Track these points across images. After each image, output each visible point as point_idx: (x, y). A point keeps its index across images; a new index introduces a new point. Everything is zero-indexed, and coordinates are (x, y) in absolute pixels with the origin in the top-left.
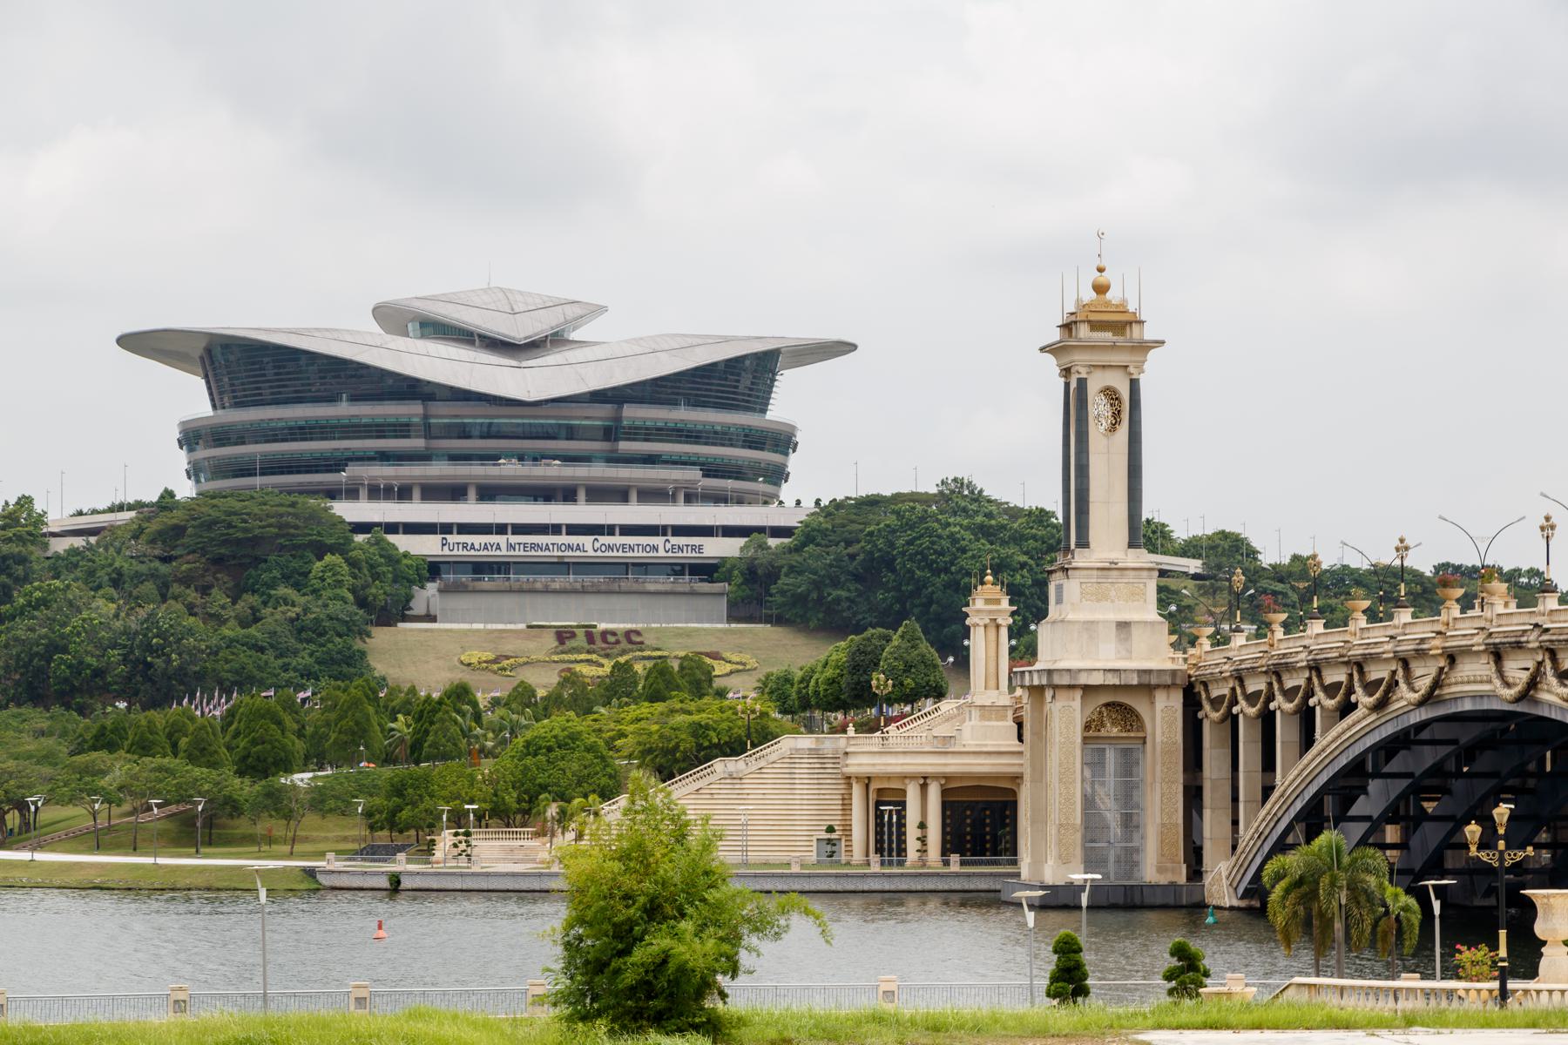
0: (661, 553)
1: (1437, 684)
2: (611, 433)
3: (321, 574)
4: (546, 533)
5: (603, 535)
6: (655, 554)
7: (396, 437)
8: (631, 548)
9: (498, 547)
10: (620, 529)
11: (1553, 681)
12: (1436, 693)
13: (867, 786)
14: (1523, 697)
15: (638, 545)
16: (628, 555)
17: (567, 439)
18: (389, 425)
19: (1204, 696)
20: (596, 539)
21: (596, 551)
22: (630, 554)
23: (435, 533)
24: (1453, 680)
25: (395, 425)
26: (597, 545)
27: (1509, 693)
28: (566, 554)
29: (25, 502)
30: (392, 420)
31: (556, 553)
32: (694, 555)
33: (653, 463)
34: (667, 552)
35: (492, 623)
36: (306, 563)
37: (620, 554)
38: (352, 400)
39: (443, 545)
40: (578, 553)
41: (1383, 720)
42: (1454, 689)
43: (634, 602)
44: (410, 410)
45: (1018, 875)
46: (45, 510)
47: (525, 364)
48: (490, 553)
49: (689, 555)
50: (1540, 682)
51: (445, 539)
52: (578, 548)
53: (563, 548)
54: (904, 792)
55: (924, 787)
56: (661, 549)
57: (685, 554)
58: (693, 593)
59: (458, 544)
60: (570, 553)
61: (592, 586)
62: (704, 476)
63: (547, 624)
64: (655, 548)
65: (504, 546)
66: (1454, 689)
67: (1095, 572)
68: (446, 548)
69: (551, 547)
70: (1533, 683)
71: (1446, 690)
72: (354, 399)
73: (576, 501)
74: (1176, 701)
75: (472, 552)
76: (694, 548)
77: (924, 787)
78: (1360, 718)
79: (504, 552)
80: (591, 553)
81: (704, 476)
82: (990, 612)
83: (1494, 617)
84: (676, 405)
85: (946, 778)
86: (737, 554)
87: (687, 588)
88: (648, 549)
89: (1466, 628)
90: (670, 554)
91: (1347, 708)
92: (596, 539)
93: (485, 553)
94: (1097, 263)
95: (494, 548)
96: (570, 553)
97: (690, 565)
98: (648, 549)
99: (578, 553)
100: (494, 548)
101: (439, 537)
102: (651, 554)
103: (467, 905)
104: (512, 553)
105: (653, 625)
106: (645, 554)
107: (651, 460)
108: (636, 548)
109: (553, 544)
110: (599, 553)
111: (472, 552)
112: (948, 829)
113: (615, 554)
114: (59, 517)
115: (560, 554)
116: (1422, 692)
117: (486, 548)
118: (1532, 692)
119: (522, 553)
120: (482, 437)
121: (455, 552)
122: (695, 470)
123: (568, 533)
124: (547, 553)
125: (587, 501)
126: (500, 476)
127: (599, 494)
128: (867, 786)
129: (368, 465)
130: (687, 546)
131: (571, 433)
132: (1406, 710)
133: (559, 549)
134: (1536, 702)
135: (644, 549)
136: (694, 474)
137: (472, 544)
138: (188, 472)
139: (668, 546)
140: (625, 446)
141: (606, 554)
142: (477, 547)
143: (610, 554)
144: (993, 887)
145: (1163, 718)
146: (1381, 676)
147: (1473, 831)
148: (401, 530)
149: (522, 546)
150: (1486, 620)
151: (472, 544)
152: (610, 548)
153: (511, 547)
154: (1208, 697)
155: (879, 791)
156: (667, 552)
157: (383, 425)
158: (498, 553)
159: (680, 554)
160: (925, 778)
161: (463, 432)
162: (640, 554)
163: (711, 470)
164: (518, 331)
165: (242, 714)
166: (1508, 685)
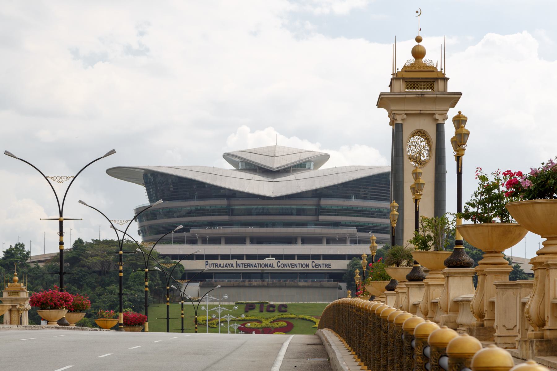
0: (311, 268)
2: (320, 211)
3: (134, 279)
4: (256, 259)
5: (283, 259)
6: (307, 268)
7: (335, 215)
8: (296, 266)
9: (232, 266)
10: (323, 257)
15: (299, 264)
16: (294, 269)
17: (297, 215)
18: (333, 210)
20: (279, 261)
21: (279, 267)
22: (295, 268)
23: (345, 259)
25: (335, 210)
26: (279, 264)
28: (264, 268)
29: (20, 247)
30: (219, 207)
31: (259, 268)
32: (326, 268)
33: (338, 226)
34: (313, 267)
35: (319, 301)
36: (128, 274)
37: (291, 268)
38: (198, 198)
39: (206, 265)
40: (270, 268)
43: (293, 291)
44: (222, 203)
46: (29, 250)
47: (276, 180)
48: (228, 268)
49: (324, 268)
51: (207, 262)
52: (270, 266)
53: (263, 266)
56: (310, 266)
57: (322, 268)
58: (322, 287)
59: (213, 264)
60: (266, 268)
61: (272, 284)
62: (358, 231)
63: (241, 302)
64: (307, 265)
65: (235, 265)
68: (208, 266)
69: (257, 265)
72: (358, 197)
73: (296, 243)
75: (220, 268)
76: (326, 265)
79: (235, 268)
80: (276, 268)
81: (358, 231)
82: (12, 301)
84: (350, 198)
86: (346, 268)
87: (318, 284)
88: (304, 266)
90: (315, 268)
92: (279, 261)
93: (226, 268)
95: (230, 266)
96: (266, 268)
97: (243, 273)
98: (304, 266)
99: (270, 268)
100: (230, 266)
101: (205, 261)
102: (305, 268)
104: (239, 268)
105: (300, 303)
106: (302, 268)
107: (337, 224)
108: (298, 265)
109: (258, 264)
110: (280, 268)
111: (220, 268)
113: (288, 268)
114: (44, 254)
115: (262, 268)
117: (226, 266)
119: (244, 268)
120: (257, 215)
121: (212, 268)
122: (354, 228)
123: (247, 259)
124: (255, 268)
125: (250, 244)
126: (308, 233)
127: (306, 240)
129: (200, 228)
130: (323, 264)
131: (300, 212)
133: (261, 266)
135: (302, 266)
136: (353, 230)
137: (220, 264)
138: (139, 232)
139: (314, 264)
140: (322, 218)
141: (284, 268)
142: (222, 265)
143: (286, 268)
148: (219, 258)
149: (243, 265)
151: (220, 264)
152: (285, 265)
153: (238, 265)
156: (313, 267)
157: (330, 210)
158: (232, 268)
159: (320, 268)
161: (249, 213)
162: (300, 268)
163: (362, 228)
164: (276, 164)
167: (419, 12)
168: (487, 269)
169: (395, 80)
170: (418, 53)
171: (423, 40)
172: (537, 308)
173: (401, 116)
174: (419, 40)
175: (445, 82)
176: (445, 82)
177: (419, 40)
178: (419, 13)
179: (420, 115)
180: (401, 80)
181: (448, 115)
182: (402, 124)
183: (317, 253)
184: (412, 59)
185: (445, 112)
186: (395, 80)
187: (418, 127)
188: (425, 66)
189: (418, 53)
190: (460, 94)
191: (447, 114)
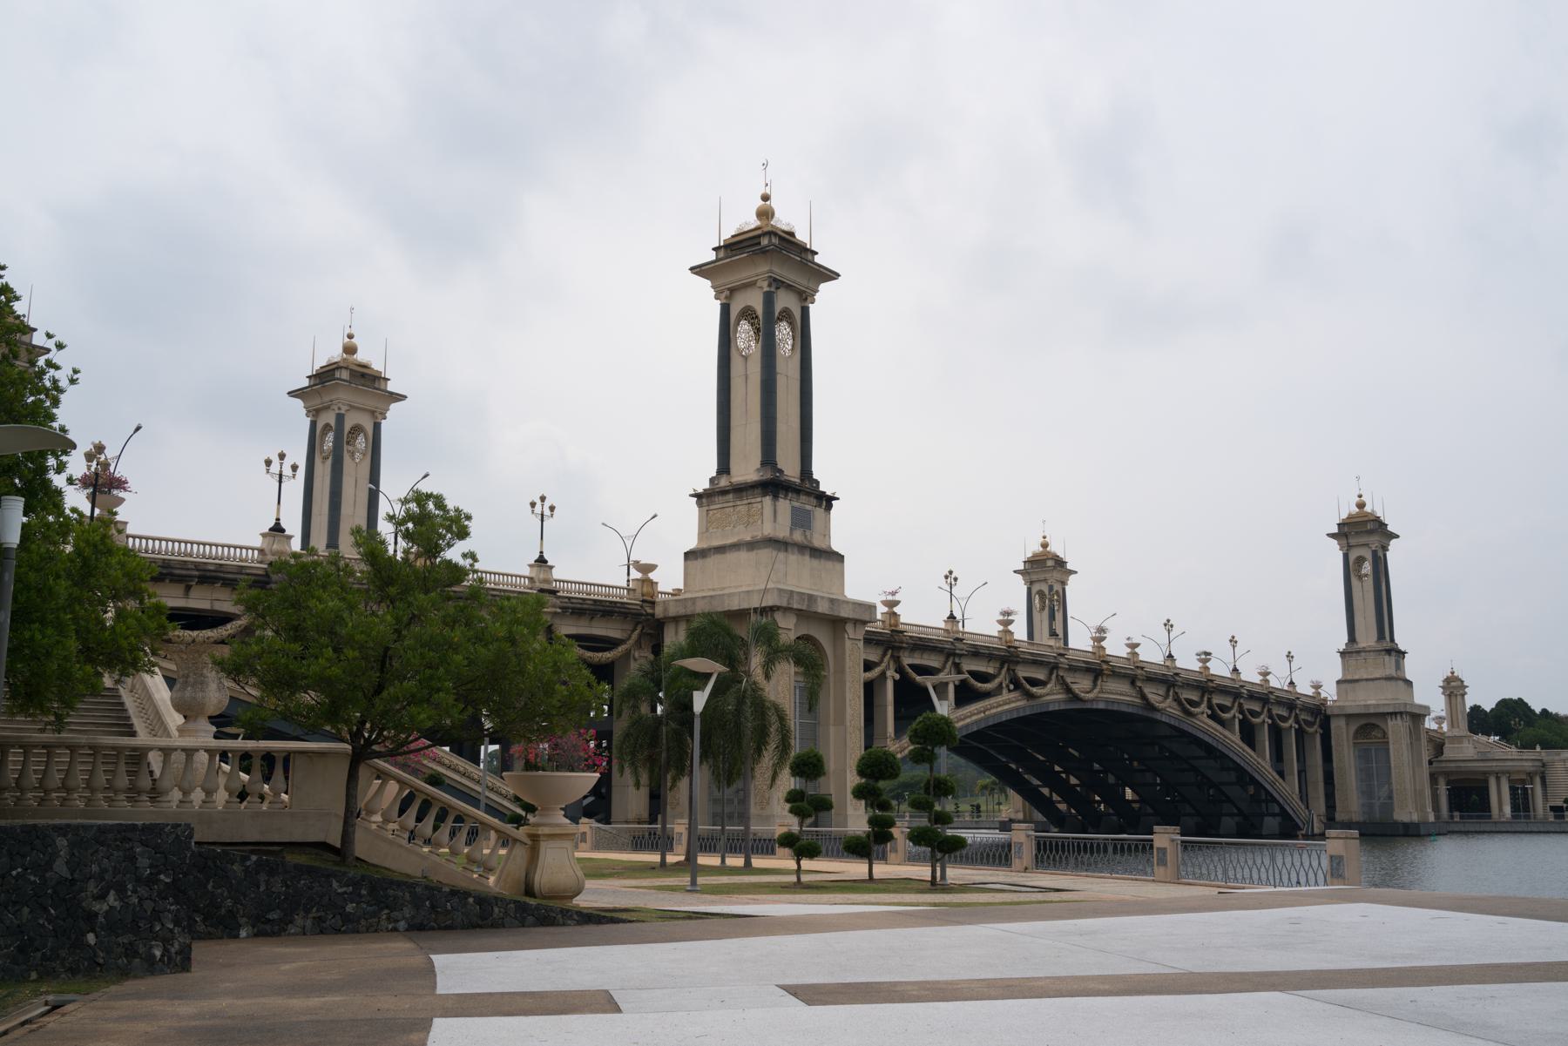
55: (1498, 779)
77: (1498, 779)
187: (1359, 555)
189: (1361, 505)
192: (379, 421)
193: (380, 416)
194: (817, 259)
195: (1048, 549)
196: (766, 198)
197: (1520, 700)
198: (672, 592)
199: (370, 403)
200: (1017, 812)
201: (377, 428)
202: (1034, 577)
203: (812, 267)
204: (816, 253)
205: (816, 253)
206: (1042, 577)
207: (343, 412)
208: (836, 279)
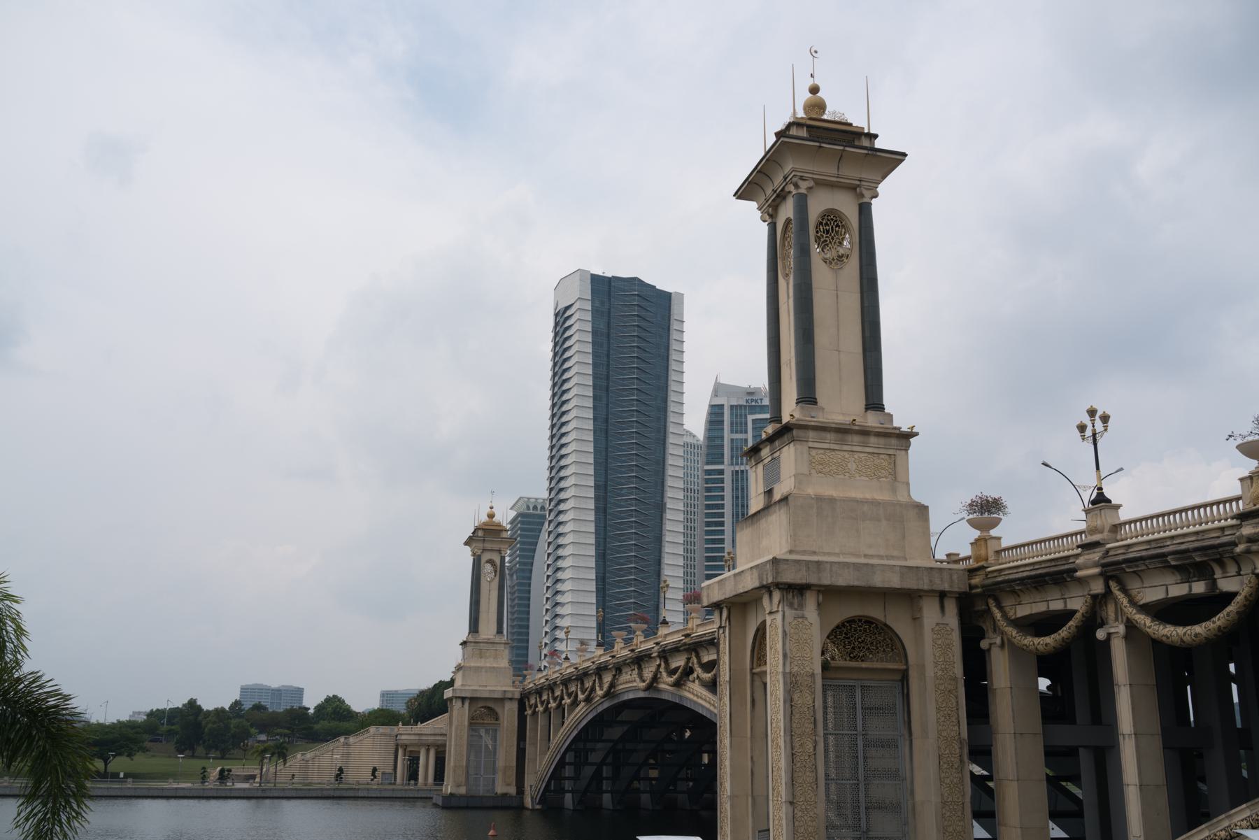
1: (612, 685)
11: (664, 674)
12: (612, 690)
13: (405, 750)
14: (650, 687)
19: (527, 704)
24: (620, 682)
27: (642, 685)
41: (591, 708)
42: (621, 687)
45: (442, 790)
50: (660, 678)
54: (419, 752)
55: (428, 751)
66: (621, 687)
67: (503, 645)
70: (655, 678)
71: (618, 688)
74: (515, 706)
77: (428, 751)
78: (581, 709)
83: (694, 627)
85: (438, 746)
89: (650, 645)
91: (575, 703)
94: (810, 82)
103: (364, 802)
112: (438, 769)
116: (648, 681)
118: (655, 685)
128: (405, 750)
132: (600, 702)
134: (658, 690)
144: (429, 796)
145: (934, 641)
146: (680, 665)
147: (242, 744)
150: (689, 629)
154: (529, 704)
155: (411, 751)
160: (429, 746)
165: (630, 627)
166: (644, 681)
167: (814, 54)
168: (39, 811)
169: (777, 595)
170: (491, 516)
171: (821, 88)
172: (1253, 805)
173: (807, 182)
174: (491, 508)
175: (871, 140)
176: (871, 140)
177: (491, 508)
178: (814, 53)
179: (492, 550)
180: (805, 129)
181: (879, 192)
182: (806, 195)
183: (886, 179)
184: (487, 519)
185: (874, 185)
186: (777, 595)
187: (490, 558)
188: (494, 522)
189: (491, 516)
190: (905, 155)
191: (878, 189)
192: (865, 200)
193: (867, 194)
194: (879, 144)
195: (494, 519)
196: (814, 90)
197: (441, 682)
198: (945, 558)
199: (851, 173)
200: (459, 786)
201: (865, 212)
202: (488, 546)
203: (742, 193)
204: (876, 136)
205: (876, 136)
206: (496, 546)
207: (803, 191)
208: (902, 161)
